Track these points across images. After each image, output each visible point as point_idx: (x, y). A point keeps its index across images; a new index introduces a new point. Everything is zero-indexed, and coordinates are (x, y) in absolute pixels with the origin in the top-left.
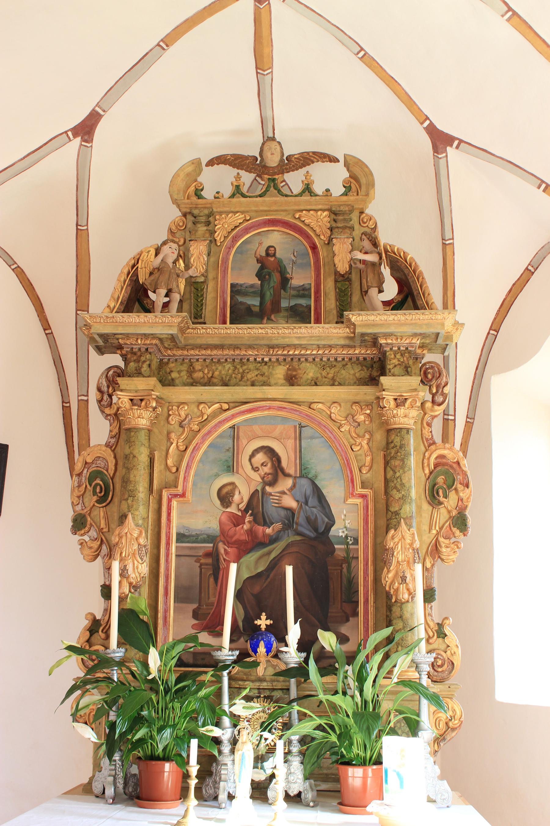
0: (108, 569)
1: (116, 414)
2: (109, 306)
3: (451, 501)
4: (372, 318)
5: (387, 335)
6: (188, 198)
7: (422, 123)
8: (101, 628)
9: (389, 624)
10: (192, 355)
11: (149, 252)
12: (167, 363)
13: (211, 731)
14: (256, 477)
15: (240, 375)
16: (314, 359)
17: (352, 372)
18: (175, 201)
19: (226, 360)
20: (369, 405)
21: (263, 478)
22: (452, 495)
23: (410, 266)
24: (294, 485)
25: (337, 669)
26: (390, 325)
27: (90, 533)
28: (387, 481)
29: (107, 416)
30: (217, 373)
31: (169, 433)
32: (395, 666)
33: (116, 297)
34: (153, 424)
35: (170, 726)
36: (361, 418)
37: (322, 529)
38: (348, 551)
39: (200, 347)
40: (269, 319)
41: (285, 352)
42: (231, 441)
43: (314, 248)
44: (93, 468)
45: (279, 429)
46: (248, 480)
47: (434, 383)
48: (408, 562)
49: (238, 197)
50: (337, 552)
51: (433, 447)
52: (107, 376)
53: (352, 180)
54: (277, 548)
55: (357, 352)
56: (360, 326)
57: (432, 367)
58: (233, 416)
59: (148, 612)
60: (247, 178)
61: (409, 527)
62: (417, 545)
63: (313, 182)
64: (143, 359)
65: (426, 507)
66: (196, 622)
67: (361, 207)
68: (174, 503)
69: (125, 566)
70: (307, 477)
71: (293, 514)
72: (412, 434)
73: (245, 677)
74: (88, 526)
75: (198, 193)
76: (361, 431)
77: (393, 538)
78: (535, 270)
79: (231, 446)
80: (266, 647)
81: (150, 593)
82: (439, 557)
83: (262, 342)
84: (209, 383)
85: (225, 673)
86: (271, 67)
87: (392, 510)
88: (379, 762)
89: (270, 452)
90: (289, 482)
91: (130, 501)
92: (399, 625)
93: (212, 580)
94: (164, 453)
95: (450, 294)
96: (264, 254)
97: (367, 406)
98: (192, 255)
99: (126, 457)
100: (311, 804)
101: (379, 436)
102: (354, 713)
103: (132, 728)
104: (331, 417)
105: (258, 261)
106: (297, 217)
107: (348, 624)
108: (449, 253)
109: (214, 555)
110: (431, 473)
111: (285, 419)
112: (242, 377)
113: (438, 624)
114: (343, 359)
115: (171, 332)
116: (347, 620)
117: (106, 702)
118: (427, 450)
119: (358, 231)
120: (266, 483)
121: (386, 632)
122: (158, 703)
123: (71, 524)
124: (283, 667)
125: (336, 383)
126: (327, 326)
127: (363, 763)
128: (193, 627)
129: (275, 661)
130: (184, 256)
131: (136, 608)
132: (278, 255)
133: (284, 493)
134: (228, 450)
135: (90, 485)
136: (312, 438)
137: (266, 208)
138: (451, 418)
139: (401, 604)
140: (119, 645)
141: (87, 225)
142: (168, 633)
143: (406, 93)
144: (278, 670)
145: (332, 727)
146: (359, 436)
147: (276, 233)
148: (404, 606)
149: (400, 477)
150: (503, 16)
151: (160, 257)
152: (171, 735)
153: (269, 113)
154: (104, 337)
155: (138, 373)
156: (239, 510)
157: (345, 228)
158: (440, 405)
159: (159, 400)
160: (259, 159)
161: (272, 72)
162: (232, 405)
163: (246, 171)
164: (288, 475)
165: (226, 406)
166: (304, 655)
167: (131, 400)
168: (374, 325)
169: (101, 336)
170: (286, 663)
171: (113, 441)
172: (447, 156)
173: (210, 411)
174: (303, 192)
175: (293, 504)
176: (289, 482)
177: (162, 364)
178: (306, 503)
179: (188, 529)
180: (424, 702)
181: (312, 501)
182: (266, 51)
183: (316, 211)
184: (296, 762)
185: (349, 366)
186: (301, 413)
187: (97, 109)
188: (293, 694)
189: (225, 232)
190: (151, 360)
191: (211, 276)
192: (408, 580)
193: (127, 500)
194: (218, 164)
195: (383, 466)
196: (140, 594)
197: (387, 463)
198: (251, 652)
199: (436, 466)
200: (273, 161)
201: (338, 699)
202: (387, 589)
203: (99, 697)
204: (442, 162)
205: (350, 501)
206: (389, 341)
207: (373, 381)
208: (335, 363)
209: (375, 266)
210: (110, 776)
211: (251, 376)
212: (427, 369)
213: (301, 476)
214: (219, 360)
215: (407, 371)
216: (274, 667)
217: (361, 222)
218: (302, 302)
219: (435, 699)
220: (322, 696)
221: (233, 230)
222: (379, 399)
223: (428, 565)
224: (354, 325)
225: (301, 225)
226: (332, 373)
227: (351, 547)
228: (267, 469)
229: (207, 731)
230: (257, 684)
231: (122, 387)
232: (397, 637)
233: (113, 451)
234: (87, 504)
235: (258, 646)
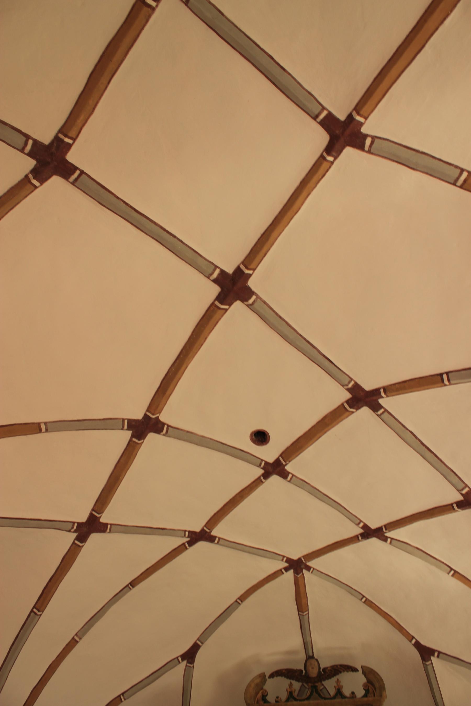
6: (258, 702)
53: (369, 685)
60: (297, 685)
86: (308, 610)
153: (308, 638)
160: (304, 672)
163: (296, 680)
182: (304, 601)
187: (198, 642)
194: (277, 676)
200: (314, 673)
204: (430, 668)
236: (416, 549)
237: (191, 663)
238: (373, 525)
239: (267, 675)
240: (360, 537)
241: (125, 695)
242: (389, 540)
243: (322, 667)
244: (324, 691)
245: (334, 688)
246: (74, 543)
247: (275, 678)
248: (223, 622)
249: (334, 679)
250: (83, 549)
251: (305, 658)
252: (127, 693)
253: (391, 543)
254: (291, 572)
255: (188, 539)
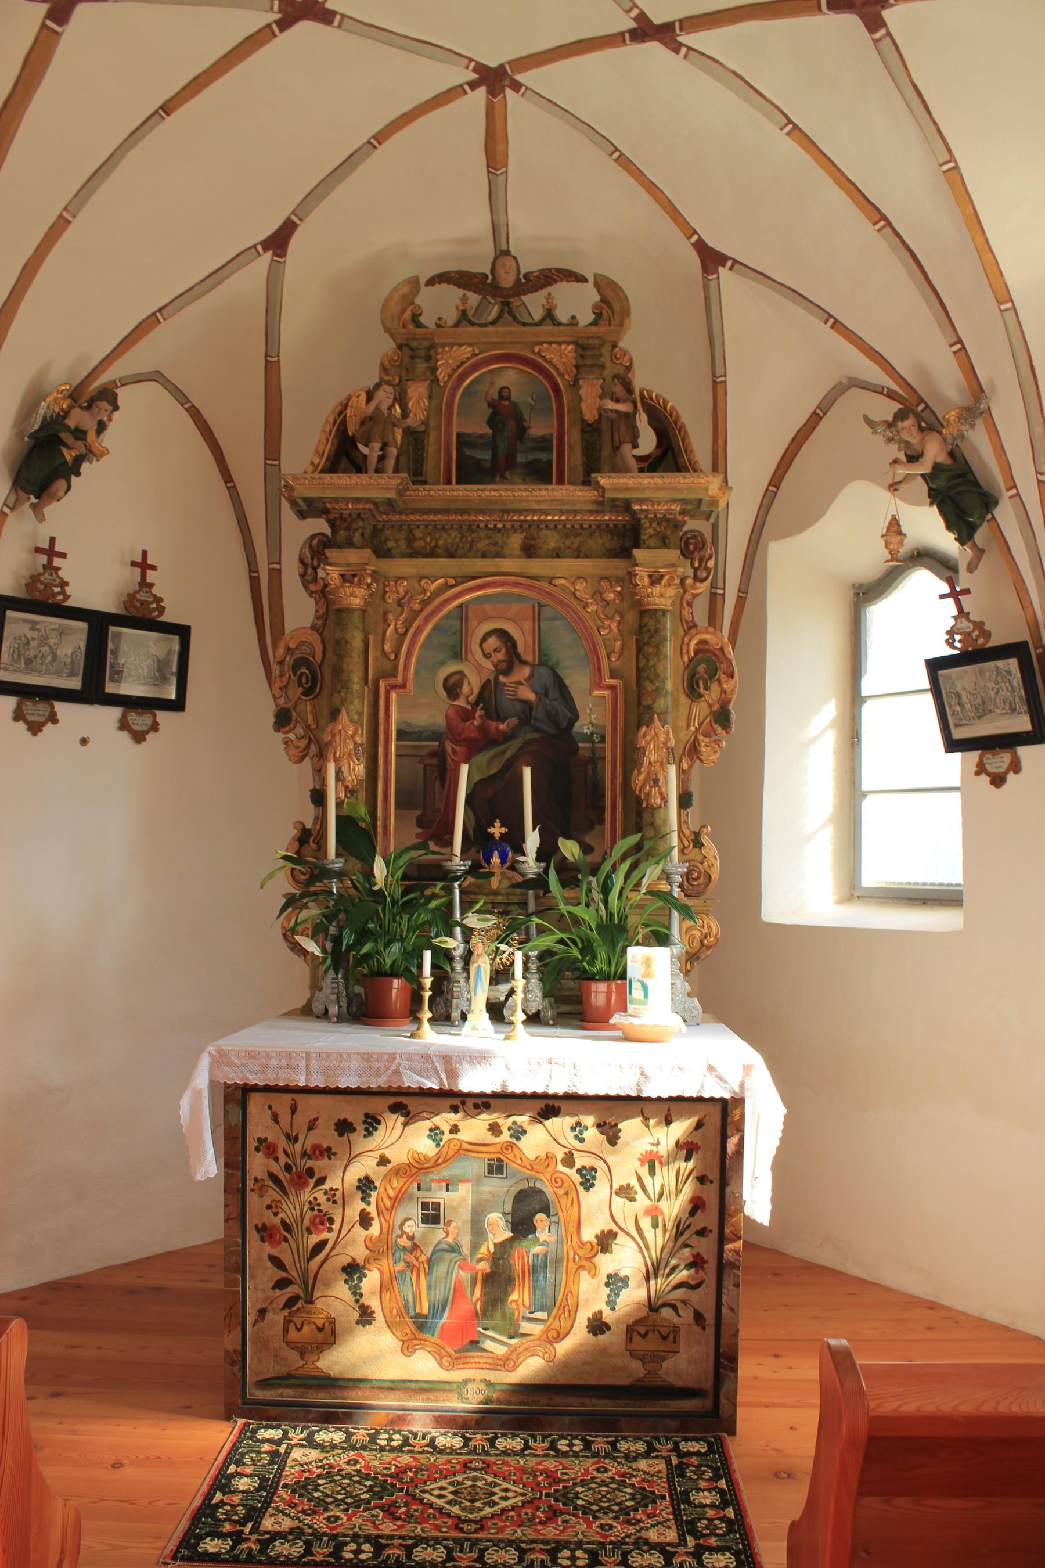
0: (320, 772)
1: (323, 591)
2: (312, 463)
3: (713, 694)
4: (625, 481)
5: (641, 501)
6: (404, 327)
7: (689, 238)
8: (312, 839)
9: (639, 830)
10: (412, 520)
11: (358, 397)
12: (382, 530)
13: (446, 942)
14: (488, 665)
15: (468, 545)
16: (556, 526)
17: (601, 541)
18: (387, 330)
19: (452, 526)
20: (619, 581)
21: (495, 666)
22: (714, 687)
23: (671, 416)
24: (532, 675)
25: (579, 880)
26: (644, 489)
27: (296, 731)
28: (639, 670)
29: (311, 593)
30: (441, 542)
31: (385, 613)
32: (644, 876)
33: (321, 451)
34: (366, 603)
35: (398, 941)
36: (611, 596)
37: (564, 725)
38: (593, 750)
39: (422, 512)
40: (503, 477)
41: (522, 518)
42: (458, 623)
43: (556, 390)
44: (298, 655)
45: (515, 608)
46: (479, 668)
47: (696, 555)
48: (662, 763)
49: (465, 326)
50: (581, 752)
51: (693, 631)
52: (310, 546)
53: (603, 305)
54: (512, 748)
55: (607, 518)
56: (611, 490)
57: (694, 537)
58: (461, 594)
59: (368, 819)
60: (474, 299)
61: (664, 722)
62: (672, 743)
63: (556, 306)
64: (354, 526)
65: (684, 700)
66: (420, 830)
67: (614, 339)
68: (393, 695)
69: (340, 768)
70: (547, 665)
71: (531, 708)
72: (668, 616)
73: (477, 890)
74: (294, 722)
75: (415, 320)
76: (610, 611)
77: (644, 736)
78: (825, 414)
79: (458, 628)
80: (500, 857)
81: (367, 798)
82: (698, 757)
83: (496, 507)
84: (432, 554)
85: (456, 884)
86: (506, 166)
87: (645, 703)
88: (623, 976)
89: (503, 635)
90: (527, 671)
91: (343, 694)
92: (650, 833)
93: (438, 783)
94: (380, 637)
95: (720, 442)
96: (496, 397)
97: (617, 582)
98: (410, 399)
99: (338, 642)
100: (551, 1022)
101: (631, 618)
102: (598, 927)
103: (359, 942)
104: (574, 594)
105: (490, 405)
106: (536, 350)
107: (593, 832)
108: (720, 393)
109: (440, 754)
110: (690, 661)
111: (521, 598)
112: (471, 547)
113: (695, 833)
114: (590, 526)
115: (388, 496)
116: (592, 828)
117: (325, 917)
118: (686, 634)
119: (610, 370)
120: (499, 672)
121: (634, 839)
122: (384, 915)
123: (273, 720)
124: (519, 879)
125: (582, 555)
126: (571, 488)
127: (607, 978)
128: (418, 836)
129: (511, 873)
130: (401, 399)
131: (355, 815)
132: (513, 398)
133: (519, 683)
134: (455, 634)
135: (295, 675)
136: (553, 619)
137: (498, 340)
138: (720, 591)
139: (652, 810)
140: (338, 855)
141: (278, 356)
142: (389, 843)
143: (670, 202)
144: (514, 881)
145: (574, 942)
146: (607, 617)
147: (510, 370)
148: (656, 812)
149: (654, 666)
150: (782, 129)
151: (373, 404)
152: (400, 950)
153: (502, 219)
154: (309, 501)
155: (350, 544)
156: (468, 703)
157: (593, 366)
158: (702, 581)
159: (375, 575)
160: (490, 277)
161: (506, 172)
162: (459, 580)
163: (475, 292)
164: (524, 663)
165: (452, 582)
166: (543, 865)
167: (342, 575)
168: (627, 489)
169: (305, 499)
170: (523, 875)
171: (319, 622)
172: (718, 278)
173: (433, 587)
174: (544, 319)
175: (531, 696)
176: (527, 671)
177: (376, 531)
178: (546, 695)
179: (409, 724)
180: (675, 914)
181: (553, 693)
182: (500, 147)
183: (560, 344)
184: (534, 981)
185: (597, 534)
186: (540, 590)
187: (293, 218)
188: (532, 907)
189: (449, 369)
190: (364, 528)
191: (432, 424)
192: (660, 783)
193: (339, 692)
194: (440, 283)
195: (634, 653)
196: (357, 799)
197: (639, 650)
198: (483, 863)
199: (696, 652)
200: (507, 280)
201: (580, 911)
202: (637, 792)
203: (319, 912)
204: (713, 285)
205: (597, 693)
206: (644, 507)
207: (624, 553)
208: (580, 531)
209: (629, 418)
210: (333, 994)
211: (482, 545)
212: (688, 539)
213: (541, 664)
214: (443, 526)
215: (664, 542)
216: (510, 879)
217: (613, 357)
218: (542, 456)
219: (686, 912)
220: (563, 908)
221: (459, 367)
222: (632, 575)
223: (685, 766)
224: (603, 488)
225: (540, 360)
226: (576, 542)
227: (597, 745)
228: (501, 656)
229: (440, 942)
230: (491, 897)
231: (331, 560)
232: (646, 847)
233: (320, 634)
234: (291, 697)
235: (491, 857)
236: (732, 75)
237: (280, 256)
238: (657, 20)
239: (423, 280)
240: (627, 36)
241: (163, 312)
242: (684, 50)
243: (523, 271)
244: (522, 309)
245: (734, 716)
246: (44, 26)
247: (437, 285)
248: (341, 180)
249: (543, 293)
250: (64, 40)
251: (493, 256)
252: (167, 309)
253: (685, 57)
254: (482, 90)
255: (278, 16)
